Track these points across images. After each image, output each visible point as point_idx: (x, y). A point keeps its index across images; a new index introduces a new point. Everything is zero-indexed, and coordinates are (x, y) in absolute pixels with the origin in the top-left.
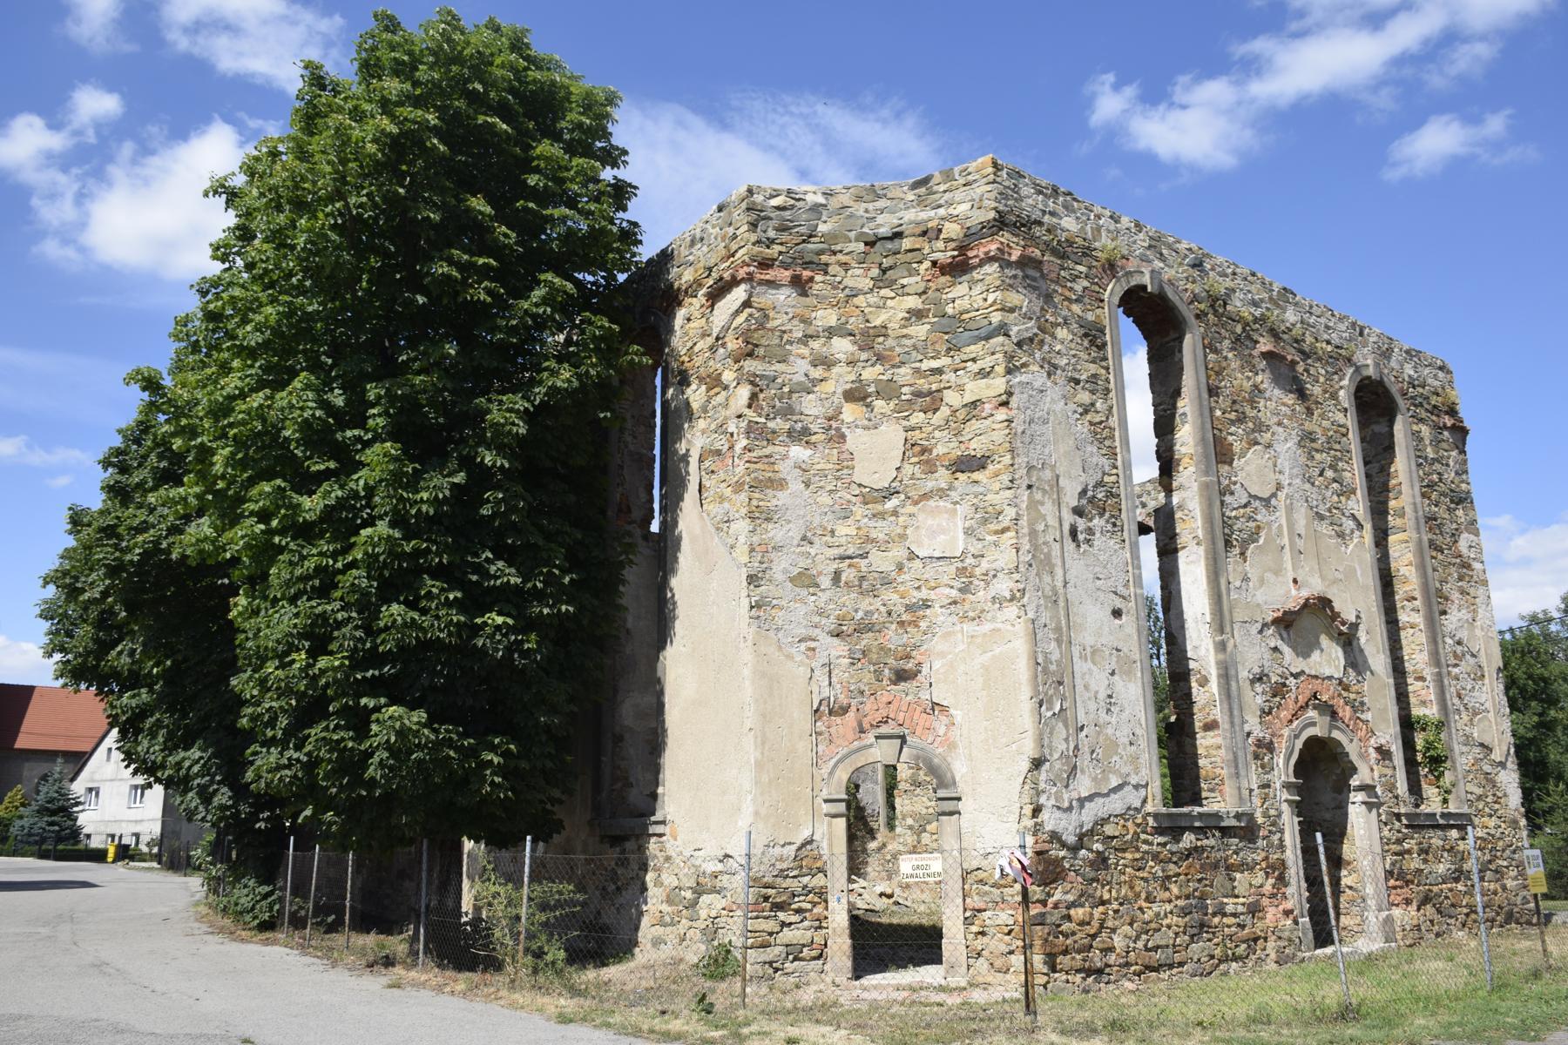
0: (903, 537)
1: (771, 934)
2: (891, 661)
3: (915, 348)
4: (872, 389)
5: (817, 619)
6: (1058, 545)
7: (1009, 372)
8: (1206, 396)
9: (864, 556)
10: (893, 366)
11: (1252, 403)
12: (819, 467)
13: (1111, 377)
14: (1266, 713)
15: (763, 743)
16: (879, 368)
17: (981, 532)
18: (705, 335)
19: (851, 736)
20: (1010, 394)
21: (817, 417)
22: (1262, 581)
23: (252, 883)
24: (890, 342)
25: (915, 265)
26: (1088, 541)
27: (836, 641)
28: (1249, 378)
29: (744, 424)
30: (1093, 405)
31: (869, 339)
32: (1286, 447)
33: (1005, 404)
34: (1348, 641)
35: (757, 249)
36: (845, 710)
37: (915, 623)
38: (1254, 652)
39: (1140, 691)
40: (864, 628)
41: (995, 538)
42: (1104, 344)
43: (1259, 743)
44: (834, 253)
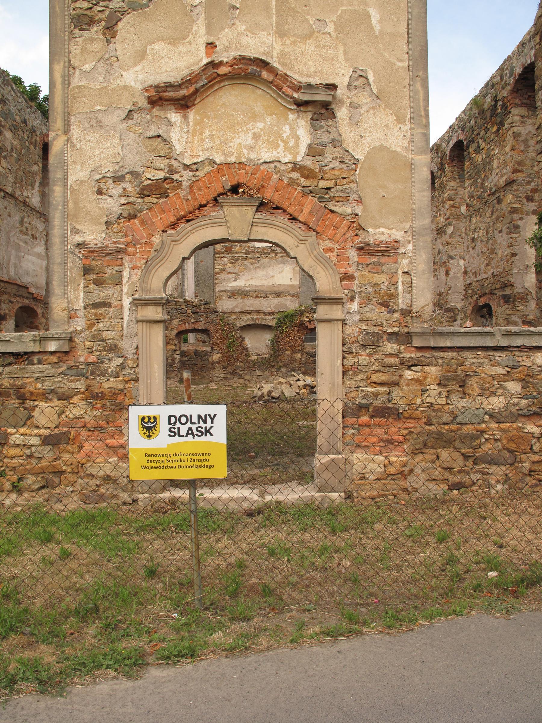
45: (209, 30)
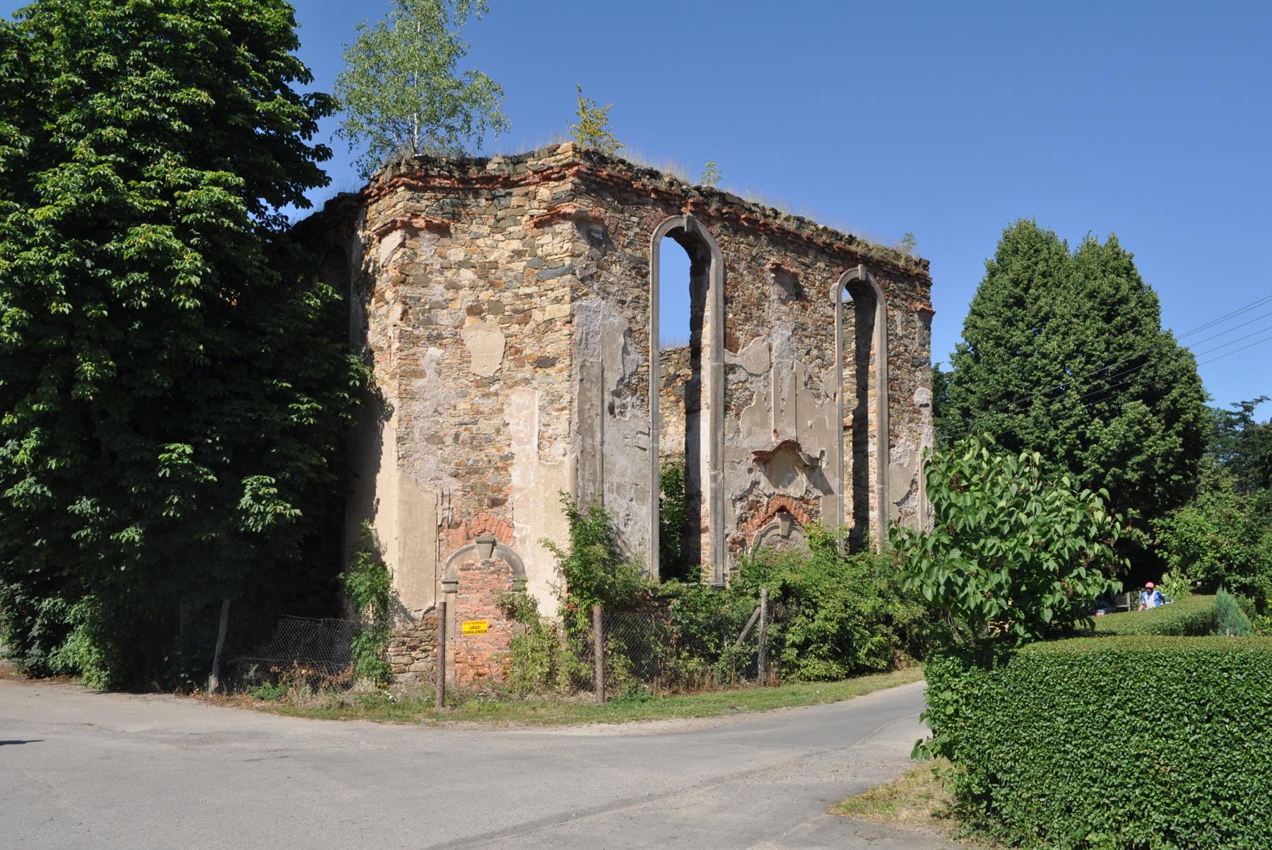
0: (501, 411)
1: (406, 665)
3: (515, 277)
5: (442, 466)
6: (599, 418)
7: (573, 299)
8: (721, 304)
9: (475, 423)
10: (500, 291)
11: (759, 306)
12: (448, 361)
13: (650, 296)
14: (742, 520)
15: (404, 547)
16: (491, 292)
17: (550, 409)
19: (461, 541)
20: (573, 315)
21: (448, 326)
22: (750, 433)
23: (95, 656)
24: (499, 273)
26: (621, 413)
27: (454, 479)
28: (758, 288)
29: (398, 332)
30: (634, 318)
31: (486, 270)
32: (780, 336)
33: (570, 322)
34: (812, 467)
35: (410, 203)
36: (458, 525)
38: (739, 480)
39: (650, 511)
40: (474, 471)
41: (557, 413)
42: (647, 273)
43: (734, 542)
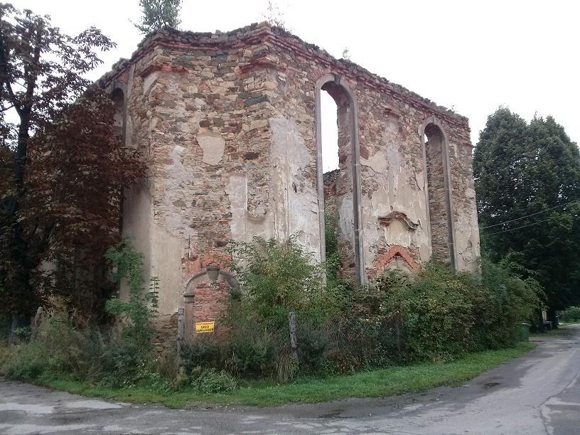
0: (223, 186)
2: (216, 238)
3: (231, 104)
4: (212, 122)
5: (185, 220)
12: (188, 155)
18: (141, 94)
19: (197, 269)
25: (232, 68)
27: (192, 230)
31: (211, 100)
32: (393, 149)
37: (226, 223)
40: (206, 224)
44: (198, 60)
45: (391, 202)
